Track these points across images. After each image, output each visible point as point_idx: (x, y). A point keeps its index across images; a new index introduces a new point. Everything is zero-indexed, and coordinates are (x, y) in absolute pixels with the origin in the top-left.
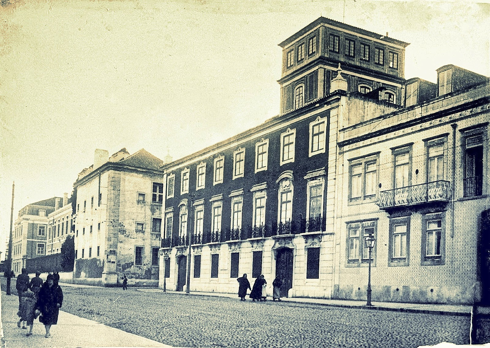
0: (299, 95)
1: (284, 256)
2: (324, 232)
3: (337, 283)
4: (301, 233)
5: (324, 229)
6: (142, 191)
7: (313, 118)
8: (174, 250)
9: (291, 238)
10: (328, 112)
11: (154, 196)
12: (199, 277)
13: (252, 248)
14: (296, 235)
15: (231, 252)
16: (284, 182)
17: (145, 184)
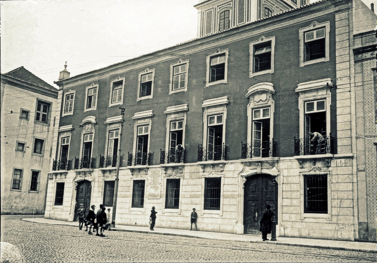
0: (224, 18)
1: (83, 187)
2: (336, 156)
3: (363, 219)
4: (295, 155)
5: (334, 150)
6: (26, 108)
7: (89, 84)
8: (72, 174)
9: (90, 173)
10: (333, 15)
11: (38, 115)
12: (62, 205)
13: (103, 178)
14: (282, 158)
15: (167, 178)
16: (87, 126)
17: (29, 101)
